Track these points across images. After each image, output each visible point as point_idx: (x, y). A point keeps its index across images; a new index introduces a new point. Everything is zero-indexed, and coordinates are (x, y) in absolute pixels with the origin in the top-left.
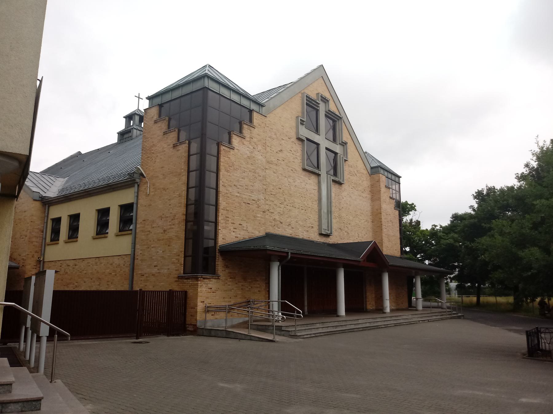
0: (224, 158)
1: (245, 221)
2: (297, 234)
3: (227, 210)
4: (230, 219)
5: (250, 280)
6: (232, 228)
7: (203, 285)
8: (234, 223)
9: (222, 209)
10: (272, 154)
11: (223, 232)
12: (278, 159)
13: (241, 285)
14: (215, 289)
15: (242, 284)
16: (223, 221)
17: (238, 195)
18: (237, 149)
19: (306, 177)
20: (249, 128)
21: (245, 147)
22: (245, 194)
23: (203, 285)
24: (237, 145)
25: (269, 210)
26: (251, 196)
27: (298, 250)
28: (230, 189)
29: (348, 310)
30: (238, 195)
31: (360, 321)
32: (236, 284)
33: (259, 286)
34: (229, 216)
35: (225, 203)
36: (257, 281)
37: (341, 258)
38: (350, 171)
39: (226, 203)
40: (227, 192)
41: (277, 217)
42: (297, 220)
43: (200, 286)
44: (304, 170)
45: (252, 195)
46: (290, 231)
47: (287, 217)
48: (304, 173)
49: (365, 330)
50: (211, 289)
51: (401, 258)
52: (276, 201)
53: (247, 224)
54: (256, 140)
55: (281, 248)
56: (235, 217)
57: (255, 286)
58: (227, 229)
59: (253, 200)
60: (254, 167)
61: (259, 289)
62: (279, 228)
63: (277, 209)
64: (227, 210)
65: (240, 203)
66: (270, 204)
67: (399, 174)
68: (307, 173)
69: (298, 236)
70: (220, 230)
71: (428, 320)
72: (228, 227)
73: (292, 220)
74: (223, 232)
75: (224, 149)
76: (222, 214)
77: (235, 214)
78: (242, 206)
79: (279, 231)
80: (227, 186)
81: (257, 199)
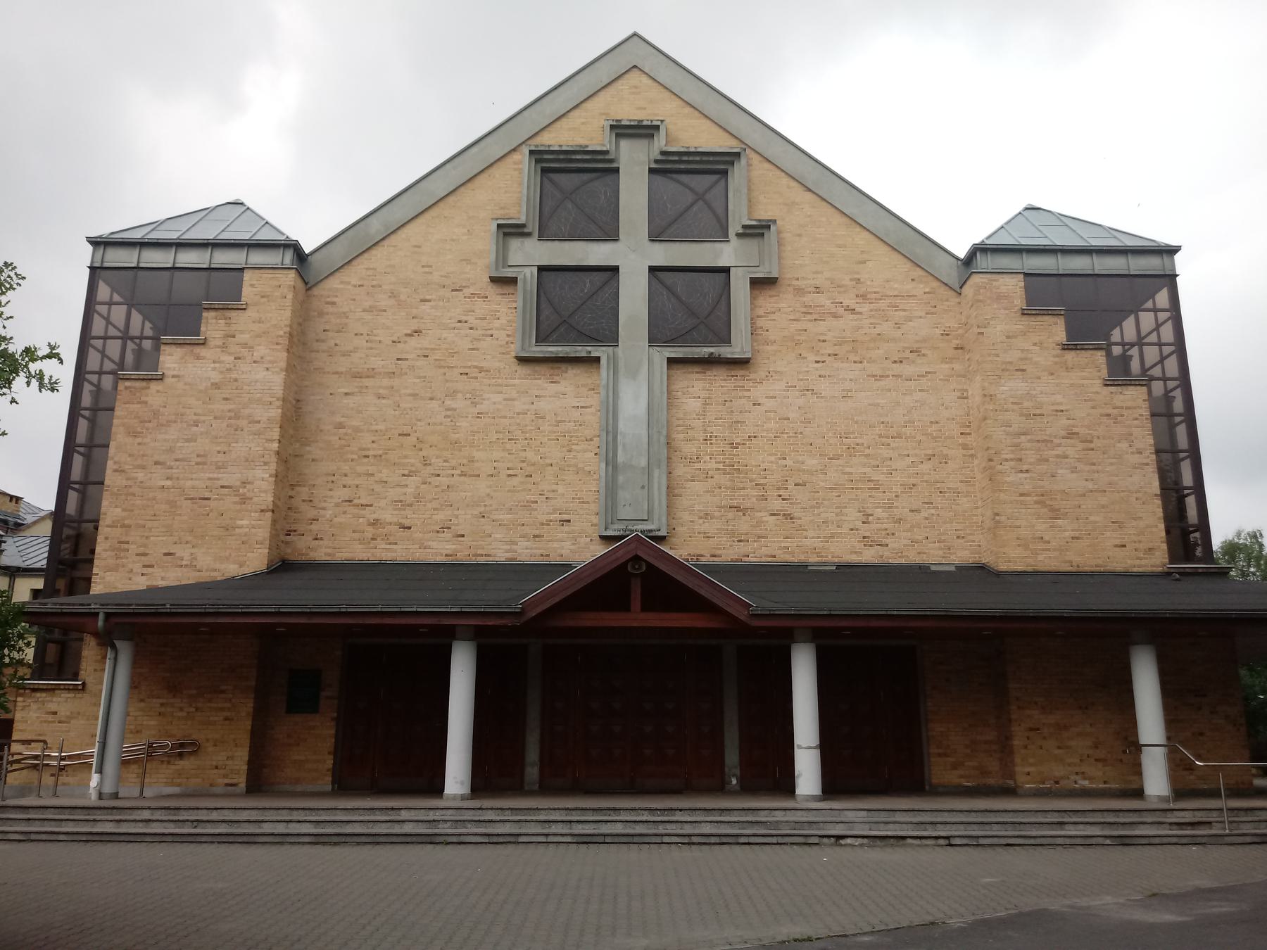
0: (127, 406)
1: (187, 543)
2: (479, 552)
3: (123, 526)
4: (133, 547)
5: (194, 692)
6: (138, 568)
7: (32, 704)
8: (145, 555)
9: (108, 526)
10: (373, 351)
11: (108, 579)
12: (398, 359)
13: (159, 705)
14: (68, 713)
15: (161, 701)
16: (108, 553)
17: (169, 483)
18: (173, 376)
19: (540, 379)
20: (224, 315)
21: (201, 365)
22: (194, 476)
23: (32, 704)
24: (174, 365)
25: (350, 501)
26: (218, 479)
27: (143, 602)
28: (140, 475)
29: (833, 786)
30: (169, 483)
31: (405, 815)
32: (142, 701)
33: (228, 705)
34: (131, 539)
35: (119, 510)
36: (223, 692)
37: (300, 610)
38: (806, 306)
39: (124, 510)
40: (129, 483)
41: (388, 515)
42: (482, 509)
43: (21, 708)
44: (523, 360)
45: (220, 475)
46: (448, 547)
47: (435, 509)
48: (523, 370)
49: (324, 843)
50: (55, 713)
51: (1168, 574)
52: (385, 471)
53: (193, 551)
54: (248, 336)
55: (158, 605)
56: (152, 538)
57: (213, 705)
58: (121, 569)
59: (222, 487)
60: (234, 403)
61: (228, 714)
62: (396, 544)
63: (387, 494)
64: (123, 526)
65: (172, 504)
66: (357, 483)
67: (1164, 237)
68: (543, 369)
69: (489, 555)
70: (97, 574)
71: (948, 838)
72: (123, 566)
73: (456, 512)
74: (108, 579)
75: (126, 388)
76: (106, 538)
77: (153, 530)
78: (181, 507)
79: (395, 551)
80: (130, 471)
81: (238, 483)
